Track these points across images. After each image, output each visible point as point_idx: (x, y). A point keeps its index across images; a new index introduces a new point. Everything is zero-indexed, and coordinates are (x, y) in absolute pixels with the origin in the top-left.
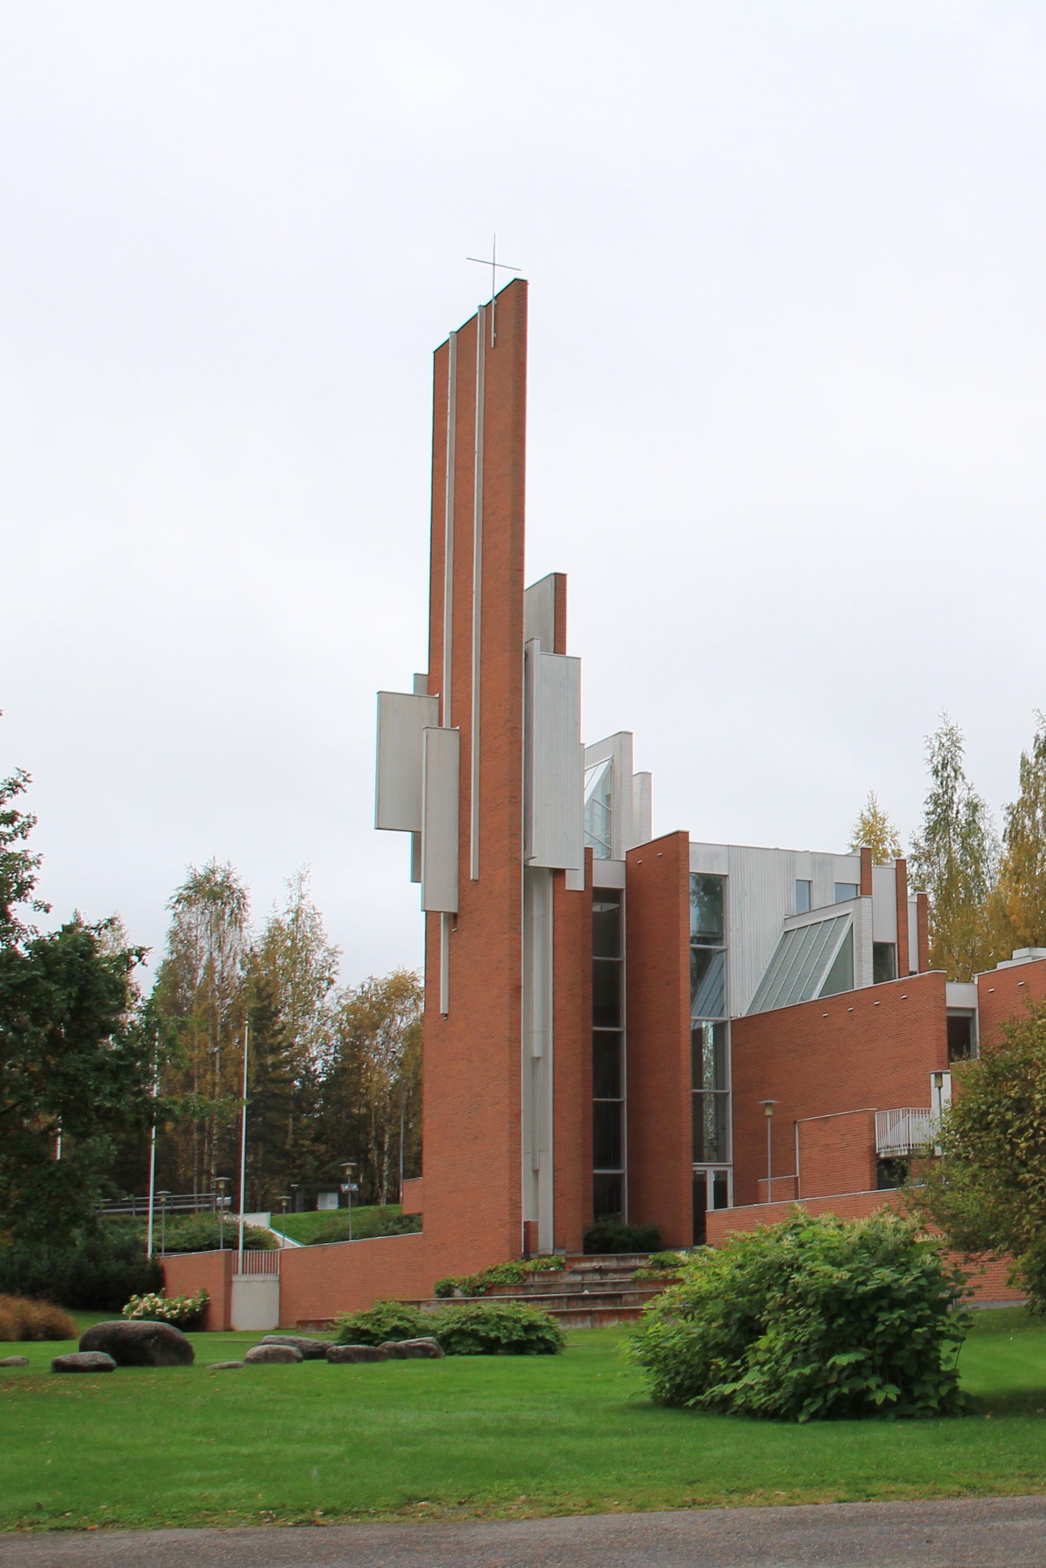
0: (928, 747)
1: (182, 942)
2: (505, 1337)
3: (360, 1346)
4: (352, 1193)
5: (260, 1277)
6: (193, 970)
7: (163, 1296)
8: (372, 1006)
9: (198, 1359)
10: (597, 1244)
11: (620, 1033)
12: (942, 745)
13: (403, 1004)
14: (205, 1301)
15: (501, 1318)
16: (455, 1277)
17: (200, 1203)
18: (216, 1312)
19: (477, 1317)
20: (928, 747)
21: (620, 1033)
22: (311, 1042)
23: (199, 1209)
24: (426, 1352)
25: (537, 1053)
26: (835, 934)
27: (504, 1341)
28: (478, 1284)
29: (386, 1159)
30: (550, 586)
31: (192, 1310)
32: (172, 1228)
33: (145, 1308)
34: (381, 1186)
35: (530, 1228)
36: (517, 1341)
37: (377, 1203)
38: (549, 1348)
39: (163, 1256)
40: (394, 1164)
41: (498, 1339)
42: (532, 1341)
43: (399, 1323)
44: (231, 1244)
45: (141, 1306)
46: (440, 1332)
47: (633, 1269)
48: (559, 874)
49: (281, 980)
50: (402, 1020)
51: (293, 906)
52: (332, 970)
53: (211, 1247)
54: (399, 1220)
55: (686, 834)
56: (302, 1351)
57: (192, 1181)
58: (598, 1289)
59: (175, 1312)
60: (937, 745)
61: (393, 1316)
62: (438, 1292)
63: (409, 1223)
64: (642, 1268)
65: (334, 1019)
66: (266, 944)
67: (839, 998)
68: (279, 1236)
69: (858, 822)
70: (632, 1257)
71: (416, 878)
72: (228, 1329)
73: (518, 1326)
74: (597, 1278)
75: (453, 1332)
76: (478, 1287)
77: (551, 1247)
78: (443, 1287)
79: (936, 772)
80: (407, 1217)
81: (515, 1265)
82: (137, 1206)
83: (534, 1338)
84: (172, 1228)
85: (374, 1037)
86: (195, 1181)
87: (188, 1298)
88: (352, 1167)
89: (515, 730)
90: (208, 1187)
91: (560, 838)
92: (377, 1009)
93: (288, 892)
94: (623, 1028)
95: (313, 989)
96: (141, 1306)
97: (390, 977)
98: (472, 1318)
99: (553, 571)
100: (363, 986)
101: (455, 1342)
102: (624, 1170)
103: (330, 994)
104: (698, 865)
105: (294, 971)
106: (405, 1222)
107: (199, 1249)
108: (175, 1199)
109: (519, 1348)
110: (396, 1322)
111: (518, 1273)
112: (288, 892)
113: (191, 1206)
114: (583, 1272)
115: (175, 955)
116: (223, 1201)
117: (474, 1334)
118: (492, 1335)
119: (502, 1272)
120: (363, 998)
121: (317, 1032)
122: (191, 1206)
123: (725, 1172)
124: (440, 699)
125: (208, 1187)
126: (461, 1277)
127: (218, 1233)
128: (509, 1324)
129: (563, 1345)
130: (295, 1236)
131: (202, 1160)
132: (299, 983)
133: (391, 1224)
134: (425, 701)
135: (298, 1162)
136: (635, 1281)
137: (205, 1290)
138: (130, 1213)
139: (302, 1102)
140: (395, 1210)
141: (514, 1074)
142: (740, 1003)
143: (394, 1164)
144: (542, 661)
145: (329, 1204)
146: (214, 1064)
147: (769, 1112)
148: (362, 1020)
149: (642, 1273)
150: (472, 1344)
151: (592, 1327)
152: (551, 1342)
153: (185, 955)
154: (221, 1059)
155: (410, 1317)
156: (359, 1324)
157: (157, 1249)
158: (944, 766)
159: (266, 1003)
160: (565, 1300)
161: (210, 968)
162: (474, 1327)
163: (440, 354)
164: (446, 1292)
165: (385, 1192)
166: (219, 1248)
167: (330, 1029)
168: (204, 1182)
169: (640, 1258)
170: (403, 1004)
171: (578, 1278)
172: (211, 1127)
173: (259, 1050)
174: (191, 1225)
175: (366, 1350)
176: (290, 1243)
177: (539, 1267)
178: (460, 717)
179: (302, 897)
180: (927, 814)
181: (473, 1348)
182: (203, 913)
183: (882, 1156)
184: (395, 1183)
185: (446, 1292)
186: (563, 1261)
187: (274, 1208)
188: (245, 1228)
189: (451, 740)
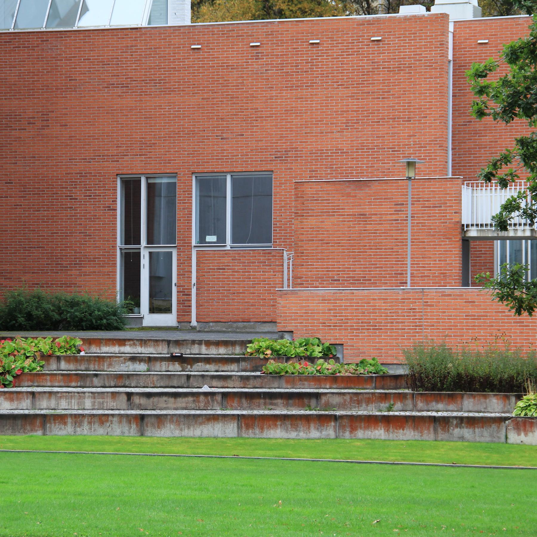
74: (176, 368)
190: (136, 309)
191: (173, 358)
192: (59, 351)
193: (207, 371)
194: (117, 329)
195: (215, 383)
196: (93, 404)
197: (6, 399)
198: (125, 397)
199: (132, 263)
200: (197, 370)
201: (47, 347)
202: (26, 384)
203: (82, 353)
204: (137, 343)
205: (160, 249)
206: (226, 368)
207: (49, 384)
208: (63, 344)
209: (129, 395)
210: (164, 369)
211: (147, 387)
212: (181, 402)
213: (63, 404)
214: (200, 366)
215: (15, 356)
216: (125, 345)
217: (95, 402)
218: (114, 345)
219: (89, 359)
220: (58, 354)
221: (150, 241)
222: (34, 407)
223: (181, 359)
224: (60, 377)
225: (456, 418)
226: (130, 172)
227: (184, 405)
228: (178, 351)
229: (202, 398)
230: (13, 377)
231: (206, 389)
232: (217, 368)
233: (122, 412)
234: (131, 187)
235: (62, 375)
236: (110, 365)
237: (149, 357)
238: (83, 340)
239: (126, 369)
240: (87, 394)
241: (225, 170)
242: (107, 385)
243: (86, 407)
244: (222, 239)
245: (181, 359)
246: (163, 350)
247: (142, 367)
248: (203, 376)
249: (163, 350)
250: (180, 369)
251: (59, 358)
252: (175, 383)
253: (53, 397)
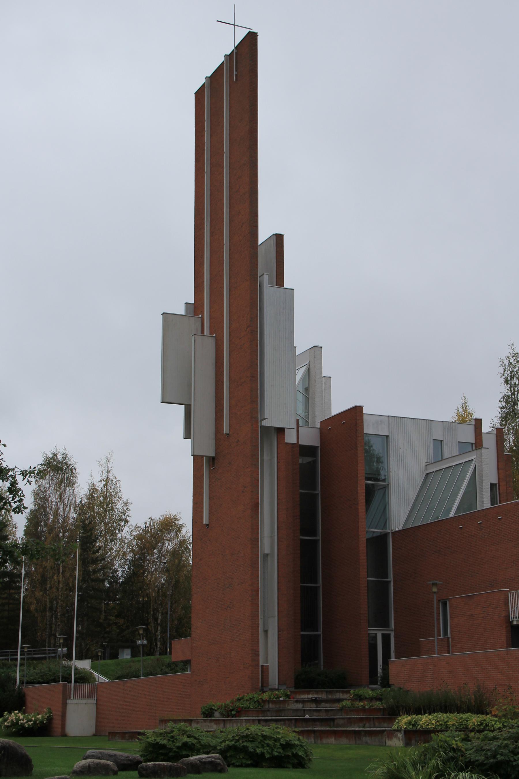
0: (501, 365)
1: (41, 498)
2: (268, 753)
3: (165, 763)
4: (143, 646)
5: (85, 701)
6: (47, 515)
7: (24, 713)
8: (152, 536)
9: (36, 769)
10: (303, 682)
11: (316, 541)
12: (510, 363)
13: (169, 534)
14: (50, 716)
15: (264, 737)
16: (216, 703)
17: (49, 653)
18: (57, 723)
19: (247, 736)
20: (501, 365)
21: (316, 541)
22: (115, 558)
23: (49, 657)
24: (214, 767)
25: (267, 551)
26: (464, 473)
27: (267, 756)
28: (231, 708)
29: (159, 628)
30: (273, 242)
31: (42, 722)
32: (32, 668)
33: (12, 721)
34: (156, 645)
35: (265, 670)
36: (277, 756)
37: (155, 655)
38: (300, 763)
39: (25, 686)
40: (164, 631)
41: (263, 754)
42: (287, 757)
43: (188, 740)
44: (67, 679)
45: (10, 719)
46: (219, 748)
47: (339, 701)
48: (280, 431)
49: (98, 521)
50: (169, 544)
51: (104, 477)
52: (127, 514)
53: (54, 681)
54: (169, 665)
55: (362, 408)
56: (116, 762)
57: (45, 641)
58: (315, 714)
59: (30, 723)
60: (507, 363)
61: (183, 734)
62: (204, 713)
63: (174, 667)
64: (346, 699)
65: (129, 544)
66: (88, 499)
67: (469, 517)
68: (96, 674)
69: (455, 415)
70: (337, 692)
71: (187, 435)
72: (64, 735)
73: (278, 744)
74: (313, 706)
75: (229, 748)
76: (231, 711)
77: (277, 683)
78: (207, 710)
79: (506, 382)
80: (174, 663)
81: (255, 696)
82: (12, 655)
83: (290, 754)
84: (32, 668)
85: (152, 554)
86: (47, 640)
87: (39, 714)
88: (144, 629)
89: (254, 332)
90: (55, 644)
91: (279, 410)
92: (154, 537)
93: (100, 469)
94: (319, 537)
95: (116, 526)
96: (10, 719)
97: (162, 518)
98: (243, 737)
99: (275, 233)
100: (146, 523)
101: (231, 756)
102: (320, 633)
103: (126, 529)
104: (368, 429)
105: (105, 515)
106: (173, 667)
107: (48, 682)
108: (34, 651)
109: (277, 763)
110: (185, 739)
111: (258, 701)
112: (100, 469)
113: (44, 655)
114: (304, 702)
115: (37, 507)
116: (62, 650)
117: (244, 750)
118: (258, 751)
119: (247, 700)
120: (146, 531)
121: (119, 551)
122: (44, 655)
123: (389, 635)
124: (202, 319)
125: (55, 644)
126: (219, 704)
127: (59, 672)
128: (271, 743)
129: (310, 760)
130: (105, 675)
131: (51, 628)
132: (109, 523)
133: (164, 668)
134: (193, 320)
135: (108, 630)
136: (342, 709)
137: (50, 709)
138: (7, 659)
139: (109, 594)
140: (166, 659)
141: (254, 564)
142: (397, 521)
143: (164, 631)
144: (269, 291)
145: (126, 655)
146: (59, 569)
147: (435, 590)
148: (145, 544)
149: (347, 703)
150: (243, 758)
151: (315, 743)
152: (303, 758)
153: (43, 506)
154: (63, 567)
155: (197, 736)
156: (158, 740)
157: (22, 682)
158: (512, 377)
159: (89, 534)
160: (293, 722)
161: (56, 514)
162: (245, 744)
163: (199, 95)
164: (209, 713)
165: (158, 649)
166: (59, 682)
167: (126, 550)
168: (52, 641)
169: (343, 692)
170: (169, 534)
171: (300, 706)
172: (57, 607)
173: (84, 562)
174: (43, 667)
175: (170, 766)
176: (102, 679)
177: (272, 697)
178: (216, 328)
179: (108, 472)
180: (501, 408)
181: (244, 761)
182: (52, 479)
183: (515, 623)
184: (164, 643)
185: (209, 713)
186: (289, 693)
187: (93, 657)
188: (76, 669)
189: (210, 343)
229: (287, 722)
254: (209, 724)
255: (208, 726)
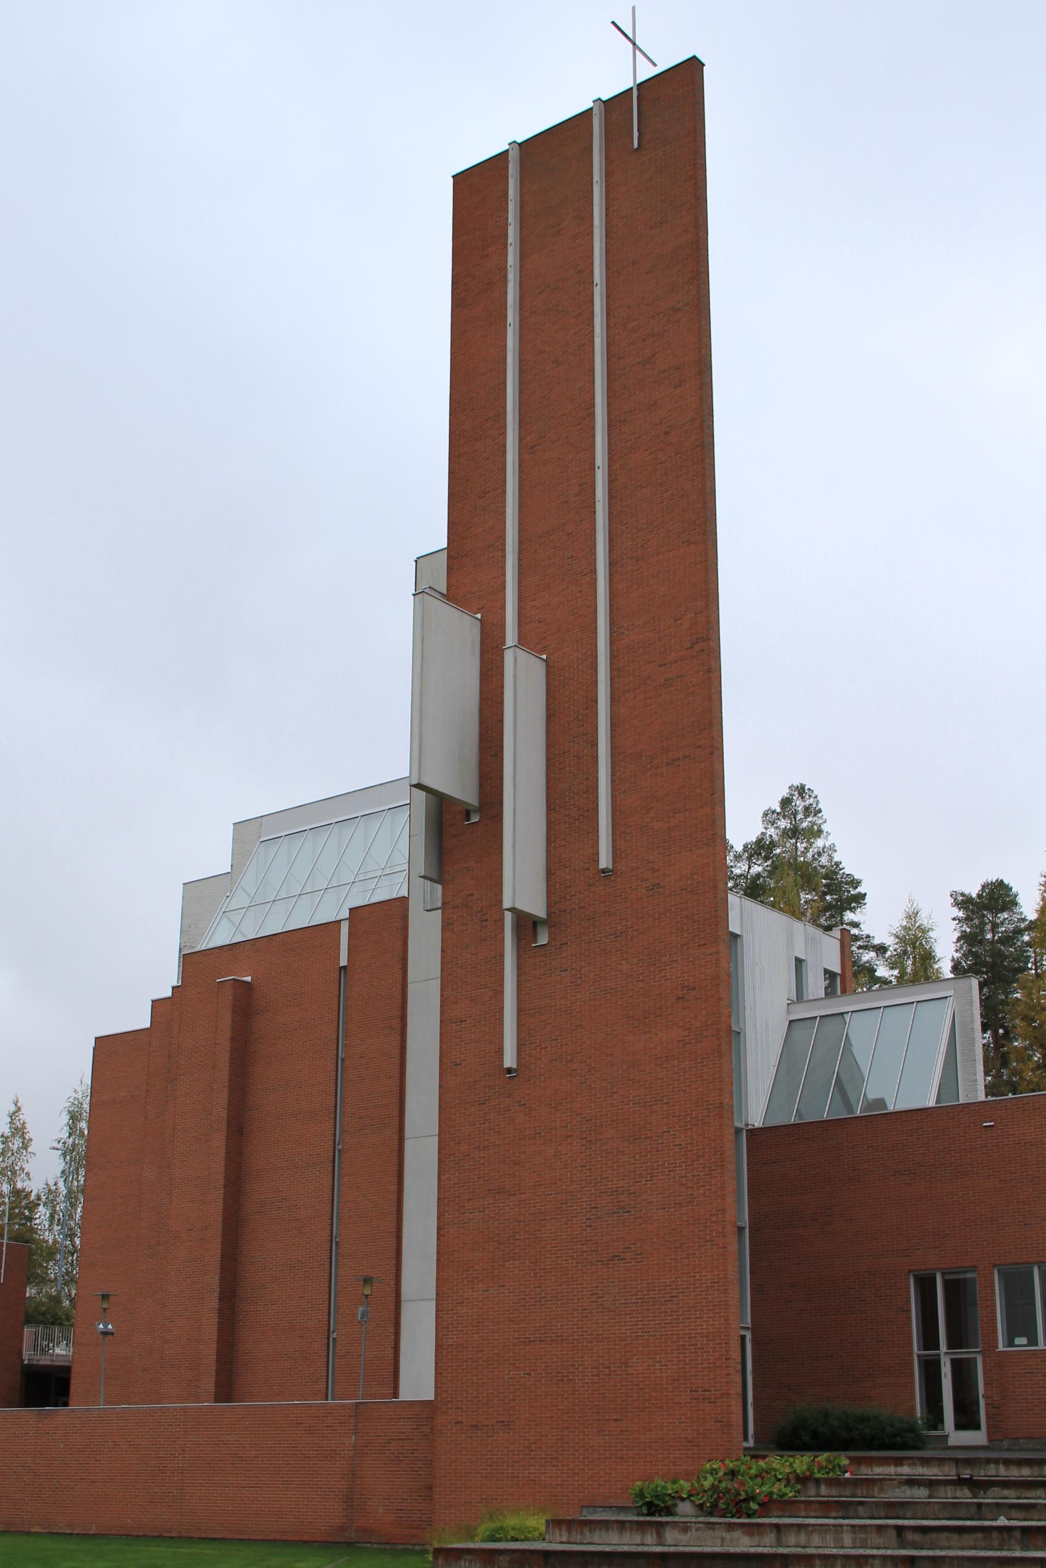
74: (964, 1495)
190: (940, 1426)
191: (960, 1482)
192: (819, 1472)
193: (1006, 1498)
194: (915, 1448)
195: (1014, 1513)
196: (854, 1540)
197: (744, 1533)
198: (893, 1533)
199: (931, 1371)
200: (988, 1499)
201: (805, 1467)
202: (775, 1514)
203: (847, 1475)
204: (918, 1462)
205: (962, 1354)
206: (1030, 1494)
207: (803, 1514)
208: (824, 1464)
209: (899, 1529)
210: (949, 1495)
211: (927, 1519)
212: (968, 1539)
213: (816, 1539)
214: (995, 1491)
215: (762, 1478)
216: (902, 1465)
217: (855, 1538)
218: (889, 1465)
219: (855, 1483)
220: (818, 1475)
221: (950, 1346)
222: (779, 1544)
223: (974, 1485)
224: (817, 1506)
225: (848, 1525)
226: (923, 1267)
227: (972, 1543)
228: (969, 1472)
229: (995, 1534)
230: (759, 1504)
231: (1002, 1521)
232: (1018, 1494)
233: (889, 1552)
234: (926, 1286)
235: (819, 1502)
236: (881, 1490)
237: (930, 1480)
238: (850, 1458)
239: (902, 1495)
240: (845, 1528)
241: (1030, 1260)
242: (876, 1515)
243: (846, 1545)
244: (1032, 1341)
245: (974, 1485)
246: (949, 1472)
247: (921, 1494)
248: (998, 1505)
249: (949, 1472)
250: (970, 1495)
251: (818, 1482)
252: (963, 1514)
253: (803, 1530)
254: (727, 1536)
255: (722, 1539)
